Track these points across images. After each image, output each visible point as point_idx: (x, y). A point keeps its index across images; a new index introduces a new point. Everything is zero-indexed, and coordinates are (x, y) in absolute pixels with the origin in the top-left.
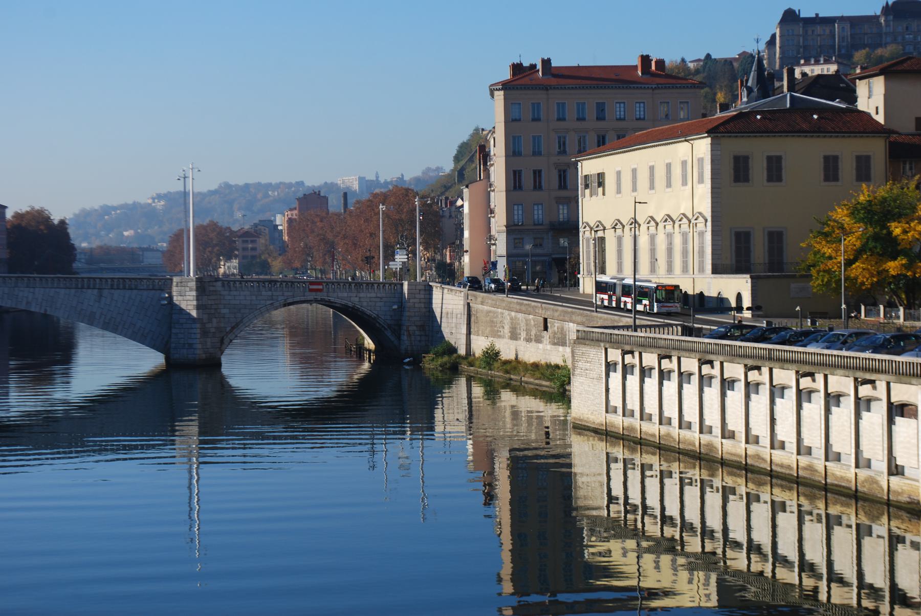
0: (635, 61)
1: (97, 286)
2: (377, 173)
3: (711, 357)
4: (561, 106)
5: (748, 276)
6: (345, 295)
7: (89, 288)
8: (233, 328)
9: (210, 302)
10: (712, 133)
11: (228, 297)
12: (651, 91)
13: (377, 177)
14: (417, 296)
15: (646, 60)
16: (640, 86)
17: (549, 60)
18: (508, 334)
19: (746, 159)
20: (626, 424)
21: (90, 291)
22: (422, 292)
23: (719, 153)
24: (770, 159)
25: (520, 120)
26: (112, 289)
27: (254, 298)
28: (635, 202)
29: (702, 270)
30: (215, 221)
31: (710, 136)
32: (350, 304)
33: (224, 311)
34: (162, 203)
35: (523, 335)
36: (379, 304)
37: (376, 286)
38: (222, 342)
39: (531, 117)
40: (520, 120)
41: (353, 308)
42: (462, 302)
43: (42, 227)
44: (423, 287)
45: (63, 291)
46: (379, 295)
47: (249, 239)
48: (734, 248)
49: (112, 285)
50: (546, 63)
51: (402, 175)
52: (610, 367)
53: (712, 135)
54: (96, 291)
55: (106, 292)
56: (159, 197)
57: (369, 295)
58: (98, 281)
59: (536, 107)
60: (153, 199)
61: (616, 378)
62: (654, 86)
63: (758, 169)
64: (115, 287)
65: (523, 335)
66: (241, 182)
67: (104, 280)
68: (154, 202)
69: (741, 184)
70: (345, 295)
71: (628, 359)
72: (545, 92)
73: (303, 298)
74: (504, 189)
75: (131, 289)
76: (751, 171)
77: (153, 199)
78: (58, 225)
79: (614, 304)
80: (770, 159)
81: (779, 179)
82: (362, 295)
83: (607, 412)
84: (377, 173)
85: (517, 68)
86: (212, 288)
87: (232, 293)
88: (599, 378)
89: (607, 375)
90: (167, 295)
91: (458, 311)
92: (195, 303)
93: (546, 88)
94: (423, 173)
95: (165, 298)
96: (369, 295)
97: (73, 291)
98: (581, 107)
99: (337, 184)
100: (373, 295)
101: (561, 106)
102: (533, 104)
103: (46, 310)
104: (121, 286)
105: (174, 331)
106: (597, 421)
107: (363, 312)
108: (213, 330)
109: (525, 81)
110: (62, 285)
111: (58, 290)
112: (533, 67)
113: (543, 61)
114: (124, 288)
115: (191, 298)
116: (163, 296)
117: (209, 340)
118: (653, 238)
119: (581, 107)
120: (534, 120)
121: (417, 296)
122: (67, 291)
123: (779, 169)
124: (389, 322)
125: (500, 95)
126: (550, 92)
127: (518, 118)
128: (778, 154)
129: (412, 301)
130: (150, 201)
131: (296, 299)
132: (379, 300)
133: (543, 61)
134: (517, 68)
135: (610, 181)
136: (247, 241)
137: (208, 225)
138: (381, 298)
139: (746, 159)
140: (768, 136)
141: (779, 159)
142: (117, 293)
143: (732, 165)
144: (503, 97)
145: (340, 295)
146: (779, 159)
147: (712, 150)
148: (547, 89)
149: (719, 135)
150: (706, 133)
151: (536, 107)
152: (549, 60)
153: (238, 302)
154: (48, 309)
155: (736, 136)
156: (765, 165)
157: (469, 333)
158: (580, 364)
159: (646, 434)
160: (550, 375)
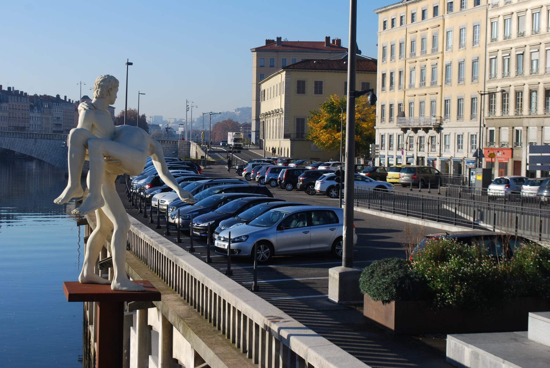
1: (34, 137)
5: (289, 139)
7: (30, 138)
10: (285, 69)
12: (329, 54)
14: (184, 147)
15: (328, 39)
16: (323, 51)
17: (281, 38)
19: (304, 82)
21: (31, 139)
22: (186, 146)
23: (289, 79)
24: (316, 83)
25: (264, 66)
26: (42, 139)
28: (139, 94)
29: (282, 137)
30: (231, 119)
31: (285, 70)
36: (167, 151)
37: (166, 142)
40: (264, 66)
43: (132, 118)
44: (187, 143)
45: (18, 139)
46: (168, 146)
47: (247, 128)
48: (296, 126)
49: (41, 137)
50: (279, 39)
53: (286, 70)
54: (34, 139)
55: (38, 141)
56: (238, 109)
58: (34, 135)
59: (272, 60)
60: (236, 110)
62: (330, 52)
63: (310, 87)
64: (43, 138)
68: (236, 112)
69: (301, 95)
72: (277, 53)
74: (255, 99)
75: (51, 139)
76: (306, 88)
77: (236, 110)
79: (60, 138)
80: (316, 83)
81: (321, 93)
85: (268, 42)
90: (65, 143)
93: (277, 51)
95: (64, 144)
97: (23, 139)
100: (165, 146)
102: (271, 59)
103: (10, 148)
104: (46, 138)
110: (17, 136)
111: (16, 138)
113: (278, 38)
114: (47, 139)
116: (62, 143)
120: (271, 66)
121: (184, 147)
122: (20, 139)
123: (321, 88)
126: (279, 53)
127: (263, 65)
128: (321, 80)
129: (181, 149)
130: (234, 111)
132: (167, 148)
133: (278, 38)
134: (268, 42)
136: (246, 129)
137: (228, 121)
138: (169, 148)
139: (304, 82)
140: (335, 72)
141: (321, 83)
142: (43, 141)
143: (296, 85)
144: (256, 55)
146: (321, 83)
147: (286, 77)
148: (277, 52)
149: (289, 70)
150: (282, 69)
151: (272, 60)
152: (281, 38)
154: (11, 147)
155: (299, 71)
156: (314, 86)
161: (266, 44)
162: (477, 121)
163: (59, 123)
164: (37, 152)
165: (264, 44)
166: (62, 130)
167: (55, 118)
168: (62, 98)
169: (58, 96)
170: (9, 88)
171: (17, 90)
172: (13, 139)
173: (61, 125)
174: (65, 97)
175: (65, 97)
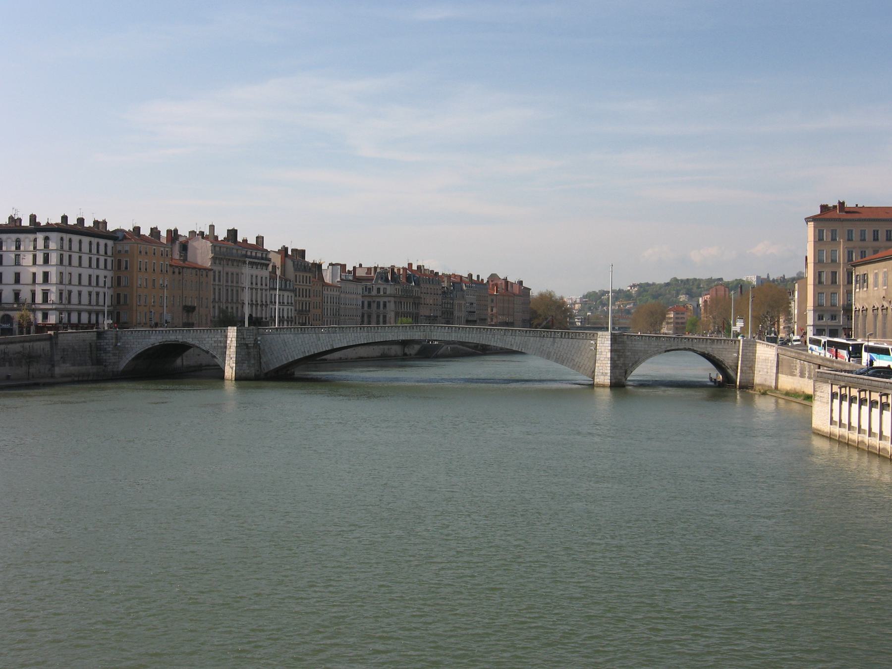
0: (836, 204)
2: (768, 274)
3: (887, 391)
4: (850, 232)
6: (703, 346)
8: (633, 364)
9: (619, 348)
11: (630, 345)
13: (768, 277)
18: (799, 374)
20: (841, 433)
21: (548, 339)
27: (646, 346)
32: (706, 352)
33: (629, 354)
34: (636, 289)
35: (807, 375)
38: (626, 373)
39: (859, 239)
41: (708, 354)
42: (774, 353)
45: (532, 338)
51: (784, 276)
52: (834, 396)
54: (552, 339)
56: (634, 286)
57: (718, 347)
60: (631, 287)
61: (836, 402)
63: (856, 236)
65: (807, 375)
66: (684, 277)
67: (690, 340)
70: (703, 346)
71: (863, 394)
73: (677, 348)
77: (631, 287)
78: (536, 299)
82: (714, 346)
83: (831, 424)
84: (768, 274)
85: (824, 208)
86: (620, 340)
87: (633, 343)
88: (827, 403)
89: (832, 401)
91: (772, 359)
92: (610, 348)
94: (797, 274)
96: (718, 347)
98: (863, 233)
99: (743, 280)
101: (850, 232)
102: (861, 231)
105: (597, 365)
106: (826, 430)
107: (714, 357)
108: (621, 365)
109: (827, 216)
112: (835, 207)
115: (608, 345)
117: (617, 371)
118: (266, 295)
119: (863, 233)
124: (731, 364)
125: (811, 224)
130: (629, 288)
131: (673, 348)
134: (824, 208)
135: (871, 280)
138: (726, 349)
145: (700, 346)
152: (843, 203)
153: (637, 349)
157: (777, 373)
158: (818, 393)
159: (851, 439)
160: (264, 362)
161: (821, 212)
162: (832, 422)
163: (472, 310)
164: (555, 355)
165: (818, 211)
166: (475, 319)
167: (467, 304)
168: (145, 231)
169: (137, 229)
170: (96, 223)
171: (92, 223)
172: (526, 338)
173: (474, 312)
174: (478, 276)
175: (478, 276)
